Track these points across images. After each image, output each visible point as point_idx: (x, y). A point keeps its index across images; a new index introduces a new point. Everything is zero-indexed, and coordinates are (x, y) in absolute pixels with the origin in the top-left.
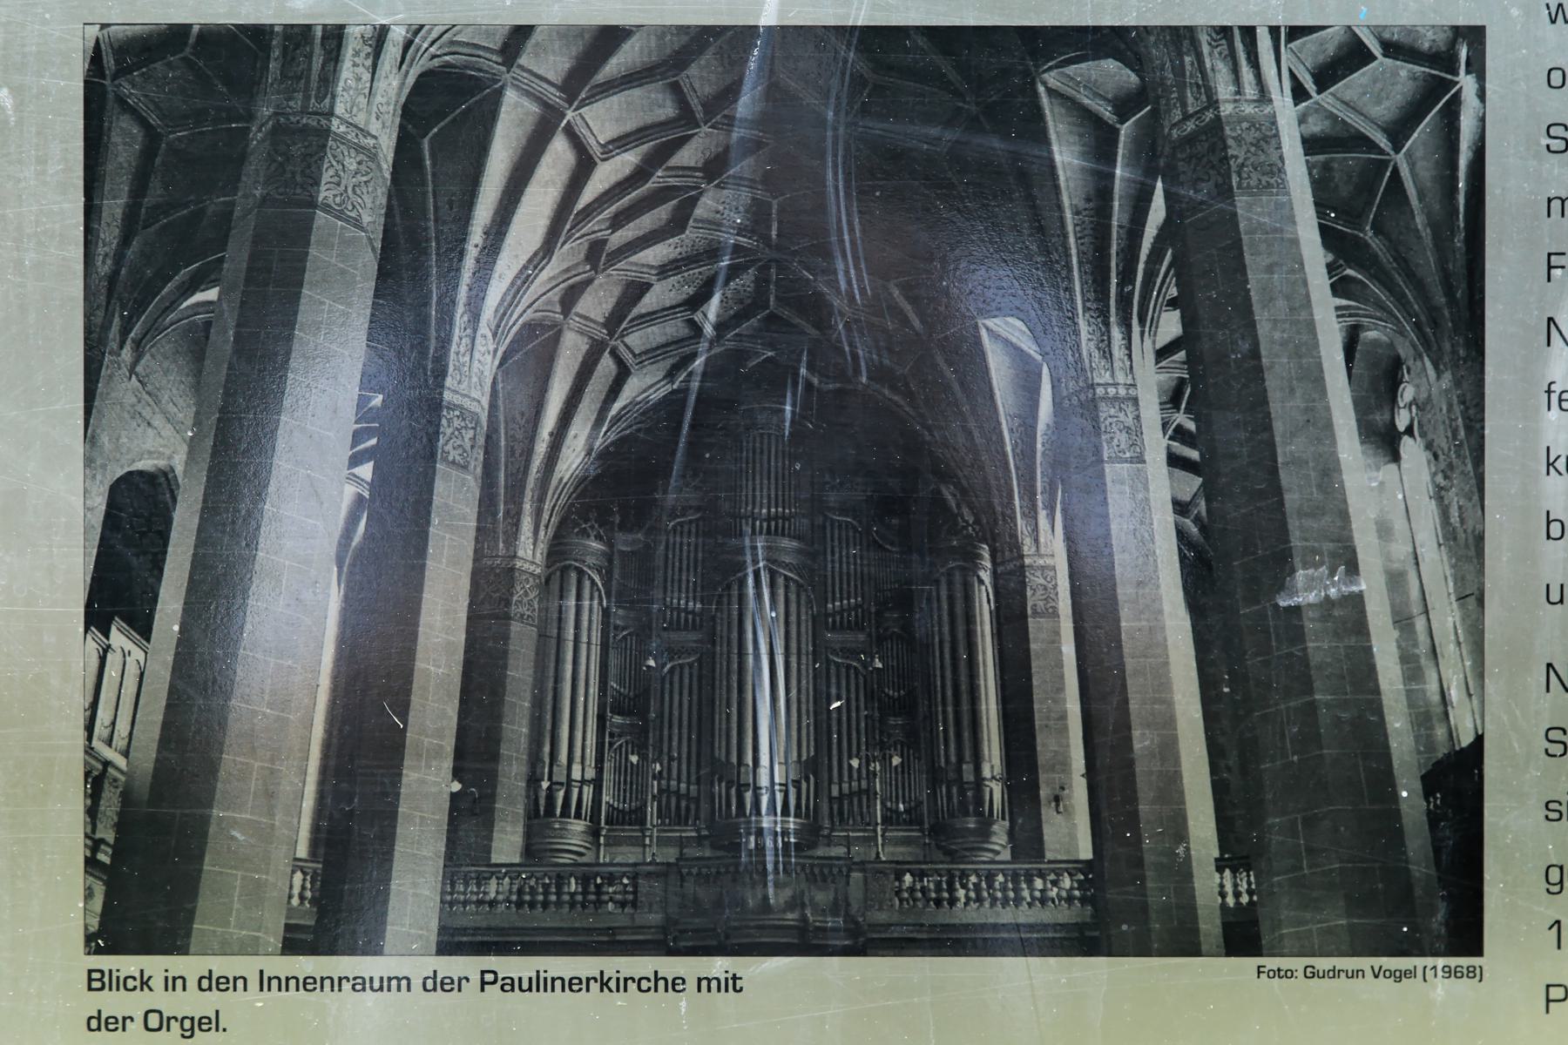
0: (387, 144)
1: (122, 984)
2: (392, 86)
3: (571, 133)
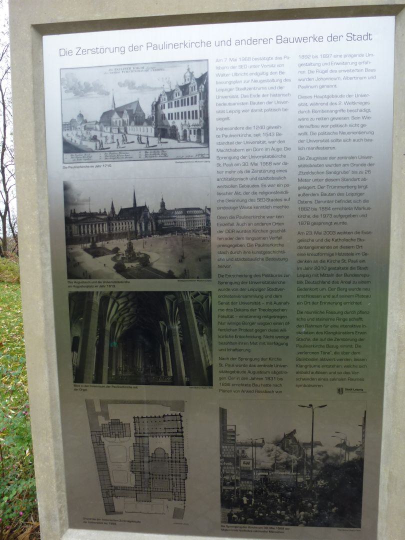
0: (99, 303)
1: (77, 386)
2: (99, 298)
3: (117, 302)
